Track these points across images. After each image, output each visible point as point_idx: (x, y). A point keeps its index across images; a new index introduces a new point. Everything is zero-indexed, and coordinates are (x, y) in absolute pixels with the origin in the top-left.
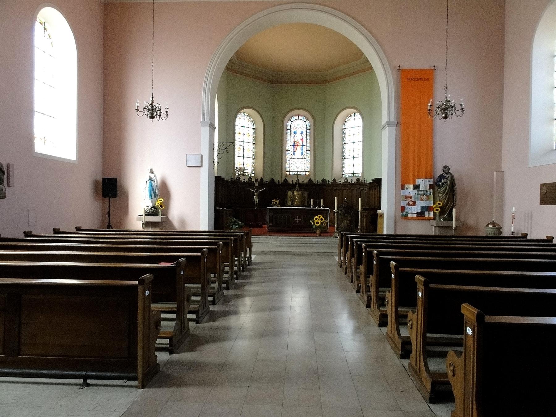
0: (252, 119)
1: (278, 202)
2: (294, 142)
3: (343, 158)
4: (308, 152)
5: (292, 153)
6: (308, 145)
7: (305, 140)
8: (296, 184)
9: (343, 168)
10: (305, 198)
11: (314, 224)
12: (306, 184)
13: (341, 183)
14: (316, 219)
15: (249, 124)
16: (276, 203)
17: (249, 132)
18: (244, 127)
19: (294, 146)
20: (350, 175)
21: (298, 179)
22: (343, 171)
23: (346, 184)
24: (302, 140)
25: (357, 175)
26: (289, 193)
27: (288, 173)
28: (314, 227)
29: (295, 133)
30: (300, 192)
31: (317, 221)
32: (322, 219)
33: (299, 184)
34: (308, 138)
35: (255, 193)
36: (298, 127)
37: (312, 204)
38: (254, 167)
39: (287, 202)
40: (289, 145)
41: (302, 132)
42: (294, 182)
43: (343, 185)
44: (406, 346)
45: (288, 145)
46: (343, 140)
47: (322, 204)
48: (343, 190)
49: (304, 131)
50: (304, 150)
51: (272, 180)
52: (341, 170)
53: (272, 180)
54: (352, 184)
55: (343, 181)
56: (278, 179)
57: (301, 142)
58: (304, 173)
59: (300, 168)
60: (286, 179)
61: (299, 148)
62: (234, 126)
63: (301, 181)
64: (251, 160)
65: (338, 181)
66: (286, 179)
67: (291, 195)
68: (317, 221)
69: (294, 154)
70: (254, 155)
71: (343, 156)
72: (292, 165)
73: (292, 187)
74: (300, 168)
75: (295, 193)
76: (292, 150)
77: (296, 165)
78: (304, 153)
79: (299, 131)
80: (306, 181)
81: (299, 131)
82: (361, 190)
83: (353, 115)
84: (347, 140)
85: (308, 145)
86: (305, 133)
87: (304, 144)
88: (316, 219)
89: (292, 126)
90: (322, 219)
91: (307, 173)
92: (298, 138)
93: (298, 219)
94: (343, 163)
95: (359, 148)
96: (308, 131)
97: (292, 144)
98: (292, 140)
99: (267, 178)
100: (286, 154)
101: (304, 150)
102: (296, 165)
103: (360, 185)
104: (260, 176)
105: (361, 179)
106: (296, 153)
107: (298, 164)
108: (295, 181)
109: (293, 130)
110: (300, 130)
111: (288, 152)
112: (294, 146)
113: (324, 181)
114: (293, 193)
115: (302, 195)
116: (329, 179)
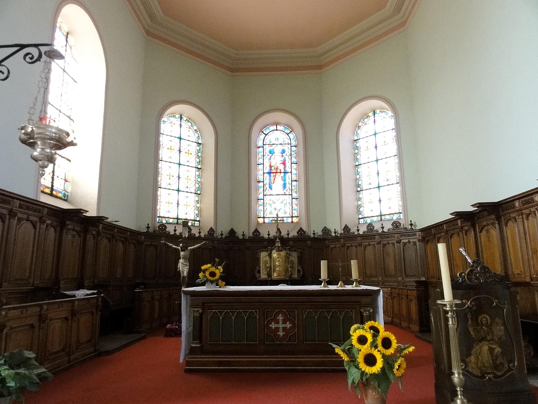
0: (195, 128)
1: (219, 271)
2: (271, 166)
3: (358, 189)
4: (294, 183)
5: (267, 186)
6: (294, 171)
7: (288, 164)
8: (275, 238)
9: (358, 207)
10: (292, 262)
11: (353, 360)
12: (294, 239)
13: (361, 232)
14: (362, 340)
15: (188, 133)
16: (213, 274)
17: (189, 148)
18: (180, 138)
19: (270, 173)
20: (375, 219)
21: (279, 230)
22: (359, 212)
23: (371, 234)
24: (284, 163)
25: (387, 217)
26: (263, 255)
27: (261, 220)
28: (353, 375)
29: (272, 152)
30: (283, 253)
31: (365, 349)
32: (387, 343)
33: (282, 239)
34: (294, 160)
35: (182, 253)
36: (276, 144)
37: (324, 275)
38: (200, 210)
39: (259, 272)
40: (261, 172)
41: (283, 152)
42: (271, 236)
43: (364, 236)
44: (275, 275)
45: (260, 173)
46: (356, 159)
47: (355, 275)
48: (365, 247)
49: (287, 148)
50: (288, 181)
51: (232, 232)
52: (355, 210)
53: (232, 232)
54: (383, 235)
55: (363, 230)
56: (243, 230)
57: (281, 167)
58: (290, 220)
59: (282, 211)
60: (256, 231)
61: (279, 177)
62: (158, 133)
63: (284, 233)
64: (193, 198)
65: (353, 230)
66: (256, 231)
67: (267, 259)
68: (365, 349)
69: (271, 188)
70: (200, 188)
71: (358, 186)
72: (267, 207)
73: (268, 244)
74: (282, 211)
75: (275, 255)
76: (267, 181)
77: (274, 206)
78: (288, 186)
79: (278, 150)
80: (294, 233)
81: (278, 150)
82: (405, 244)
83: (371, 114)
84: (363, 158)
85: (294, 171)
86: (288, 152)
87: (288, 170)
88: (362, 340)
89: (267, 141)
90: (387, 343)
91: (295, 220)
92: (277, 161)
93: (281, 325)
94: (359, 199)
95: (391, 170)
96: (294, 149)
97: (267, 170)
98: (267, 165)
99: (223, 229)
100: (257, 189)
101: (288, 181)
102: (274, 206)
103: (403, 234)
104: (209, 222)
105: (402, 222)
106: (274, 186)
107: (277, 205)
108: (273, 233)
109: (267, 148)
110: (280, 148)
111: (261, 184)
112: (270, 173)
113: (326, 231)
114: (270, 255)
115: (287, 257)
116: (336, 227)
